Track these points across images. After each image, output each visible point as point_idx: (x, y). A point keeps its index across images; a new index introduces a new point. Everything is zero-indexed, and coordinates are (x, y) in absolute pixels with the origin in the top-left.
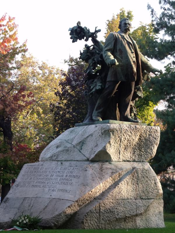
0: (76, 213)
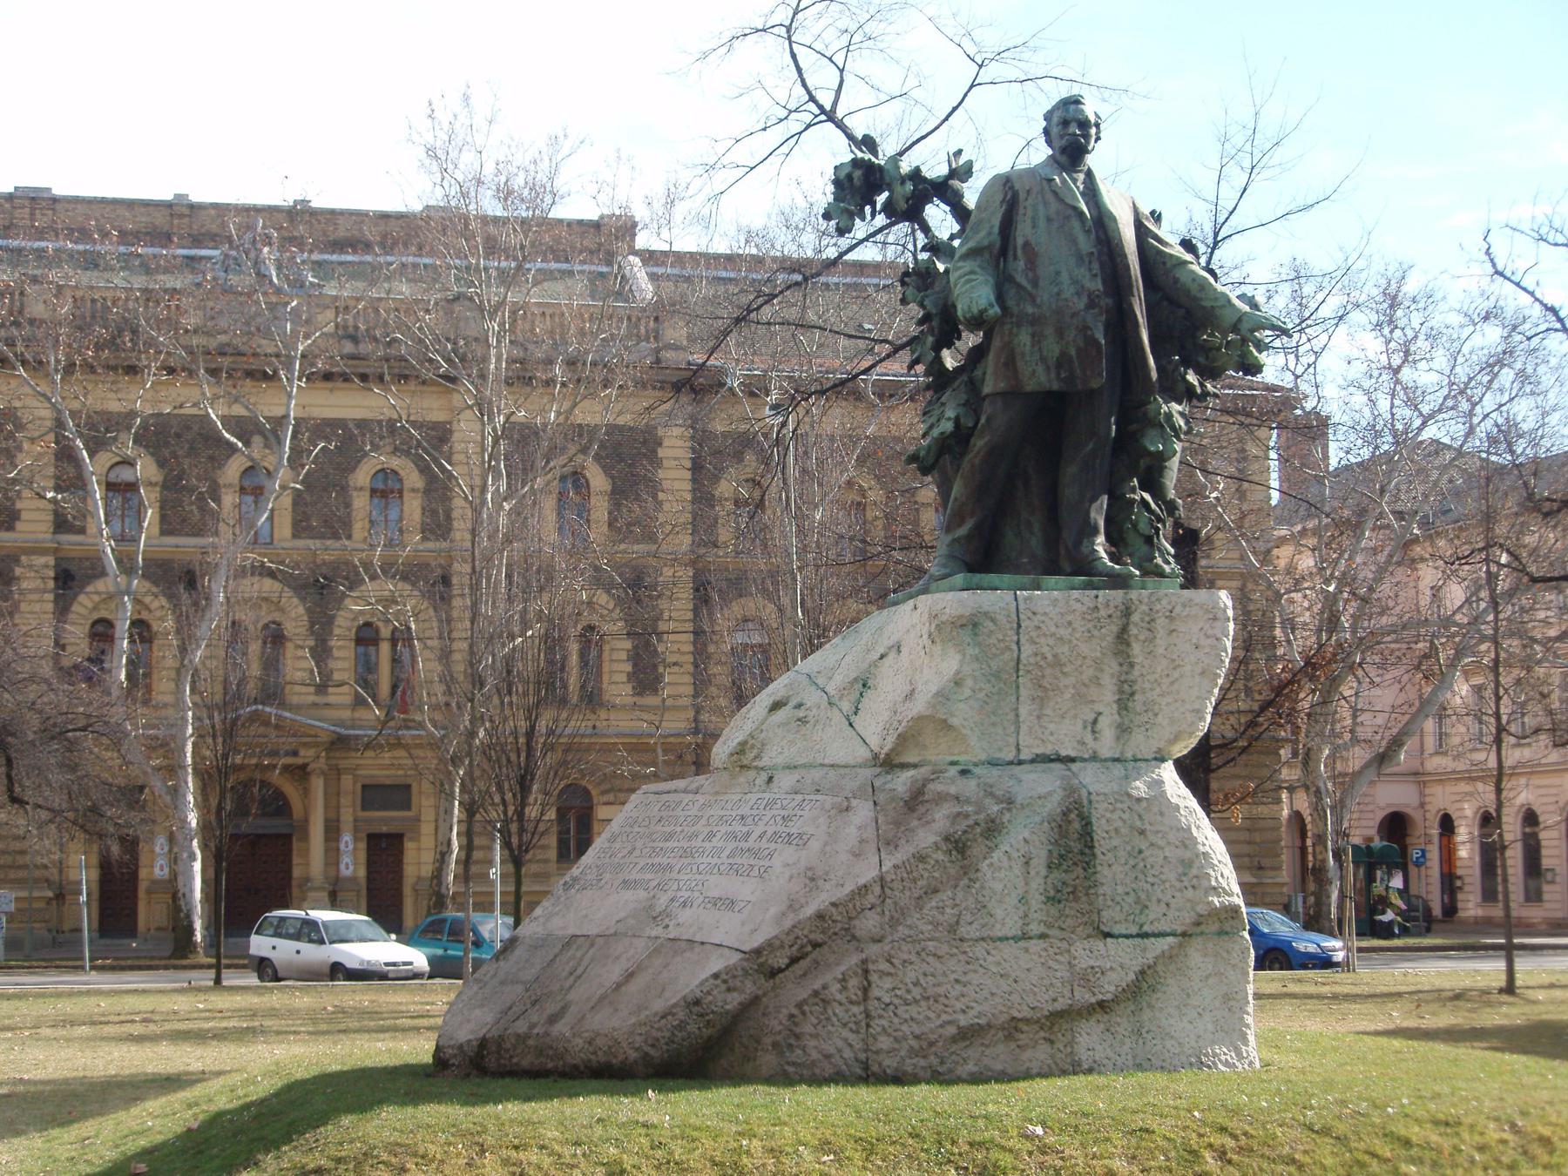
0: (438, 1049)
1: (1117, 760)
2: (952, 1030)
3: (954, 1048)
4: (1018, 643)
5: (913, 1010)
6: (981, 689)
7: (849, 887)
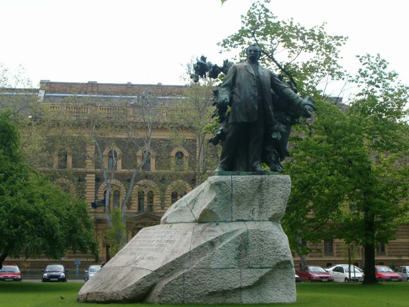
1: (259, 221)
2: (207, 293)
3: (208, 297)
4: (232, 189)
5: (197, 287)
6: (222, 202)
7: (182, 254)
